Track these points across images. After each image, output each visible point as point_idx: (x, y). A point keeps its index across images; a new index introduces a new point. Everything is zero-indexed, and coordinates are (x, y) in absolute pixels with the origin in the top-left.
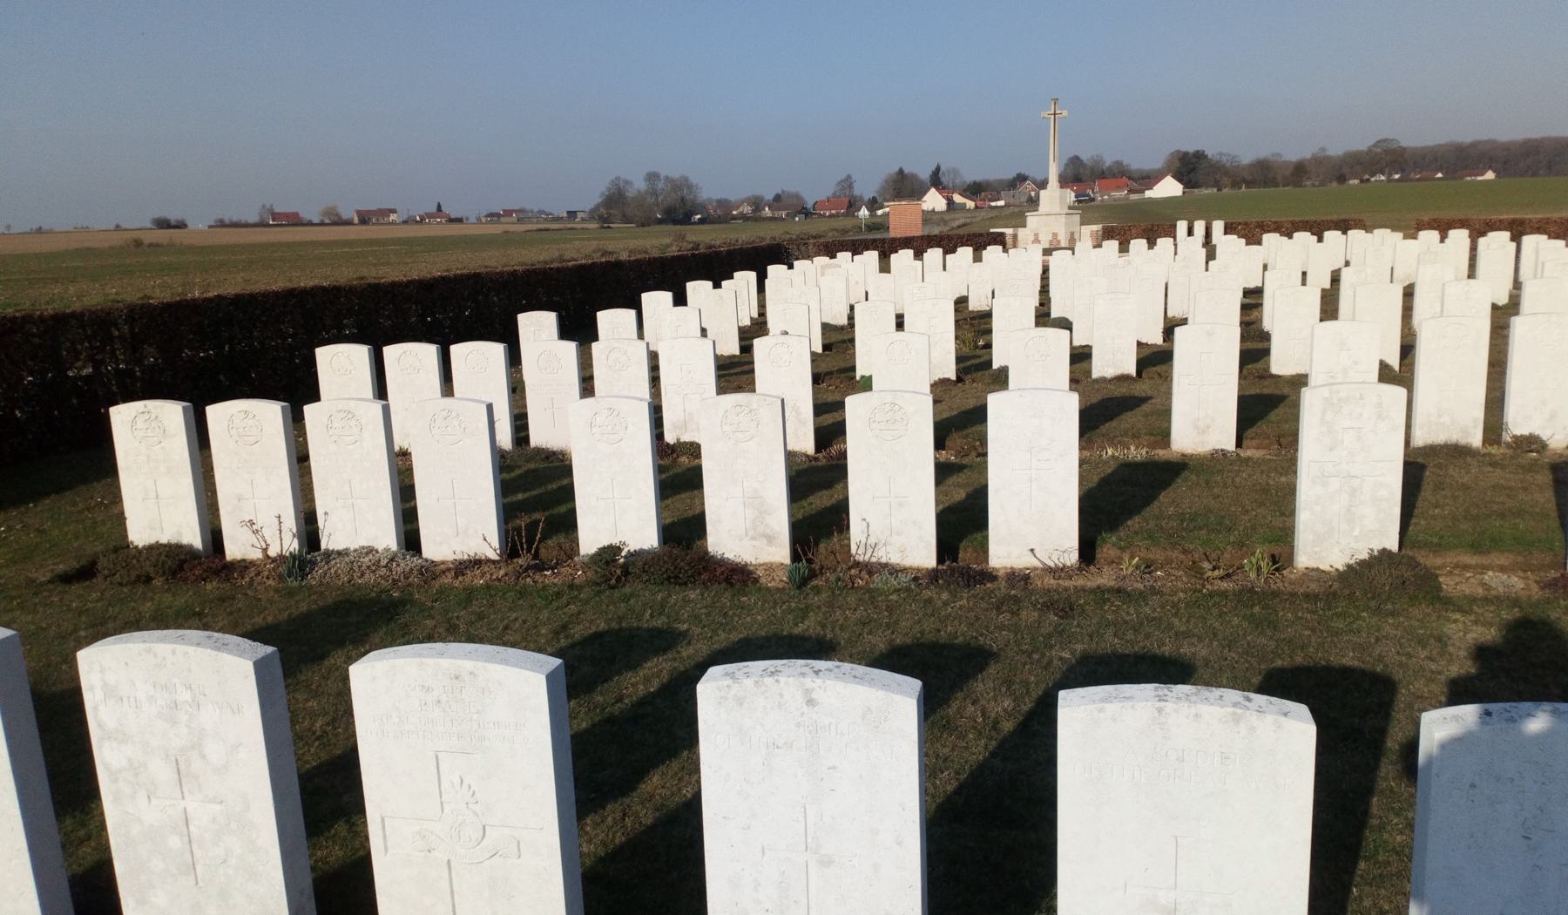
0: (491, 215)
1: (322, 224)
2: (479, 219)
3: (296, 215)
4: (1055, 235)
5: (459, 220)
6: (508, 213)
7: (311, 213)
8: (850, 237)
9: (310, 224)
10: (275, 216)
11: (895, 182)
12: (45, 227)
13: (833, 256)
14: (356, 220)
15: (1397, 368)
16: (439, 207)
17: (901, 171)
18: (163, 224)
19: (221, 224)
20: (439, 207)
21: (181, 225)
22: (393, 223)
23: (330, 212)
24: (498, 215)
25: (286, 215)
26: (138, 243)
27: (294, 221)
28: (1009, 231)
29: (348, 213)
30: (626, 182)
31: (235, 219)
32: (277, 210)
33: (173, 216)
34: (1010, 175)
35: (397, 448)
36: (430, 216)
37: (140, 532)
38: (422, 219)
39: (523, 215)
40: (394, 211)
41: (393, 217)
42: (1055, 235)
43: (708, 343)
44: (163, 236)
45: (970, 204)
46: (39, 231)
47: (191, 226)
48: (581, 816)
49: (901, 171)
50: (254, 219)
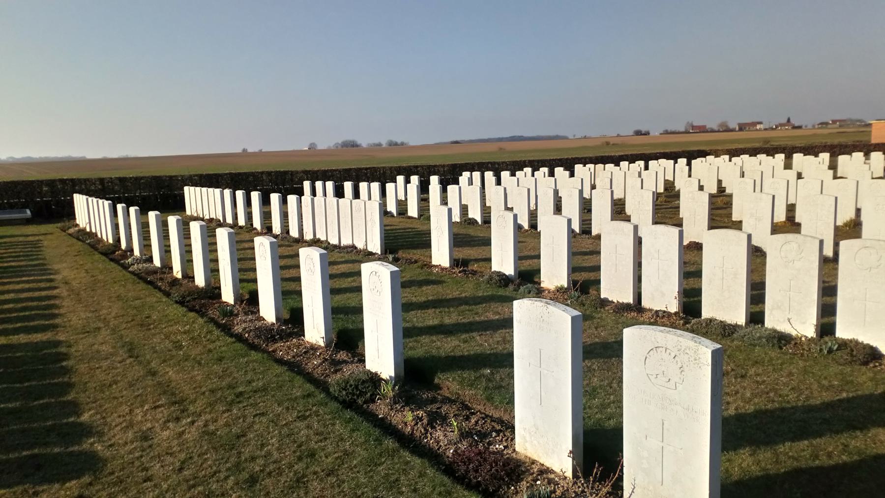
0: (822, 124)
1: (719, 131)
2: (814, 126)
3: (704, 127)
5: (800, 127)
6: (834, 122)
8: (829, 141)
9: (713, 131)
10: (693, 127)
12: (588, 135)
13: (816, 156)
14: (737, 129)
15: (719, 346)
16: (789, 120)
18: (638, 133)
19: (666, 132)
20: (789, 120)
21: (647, 133)
22: (760, 130)
23: (721, 125)
24: (827, 124)
25: (699, 127)
26: (608, 144)
27: (703, 130)
29: (733, 125)
31: (673, 130)
32: (695, 124)
33: (644, 129)
35: (685, 243)
36: (781, 125)
37: (496, 266)
38: (777, 127)
39: (843, 123)
40: (760, 123)
41: (758, 127)
43: (510, 215)
44: (640, 139)
46: (585, 137)
47: (651, 134)
48: (725, 448)
50: (683, 129)
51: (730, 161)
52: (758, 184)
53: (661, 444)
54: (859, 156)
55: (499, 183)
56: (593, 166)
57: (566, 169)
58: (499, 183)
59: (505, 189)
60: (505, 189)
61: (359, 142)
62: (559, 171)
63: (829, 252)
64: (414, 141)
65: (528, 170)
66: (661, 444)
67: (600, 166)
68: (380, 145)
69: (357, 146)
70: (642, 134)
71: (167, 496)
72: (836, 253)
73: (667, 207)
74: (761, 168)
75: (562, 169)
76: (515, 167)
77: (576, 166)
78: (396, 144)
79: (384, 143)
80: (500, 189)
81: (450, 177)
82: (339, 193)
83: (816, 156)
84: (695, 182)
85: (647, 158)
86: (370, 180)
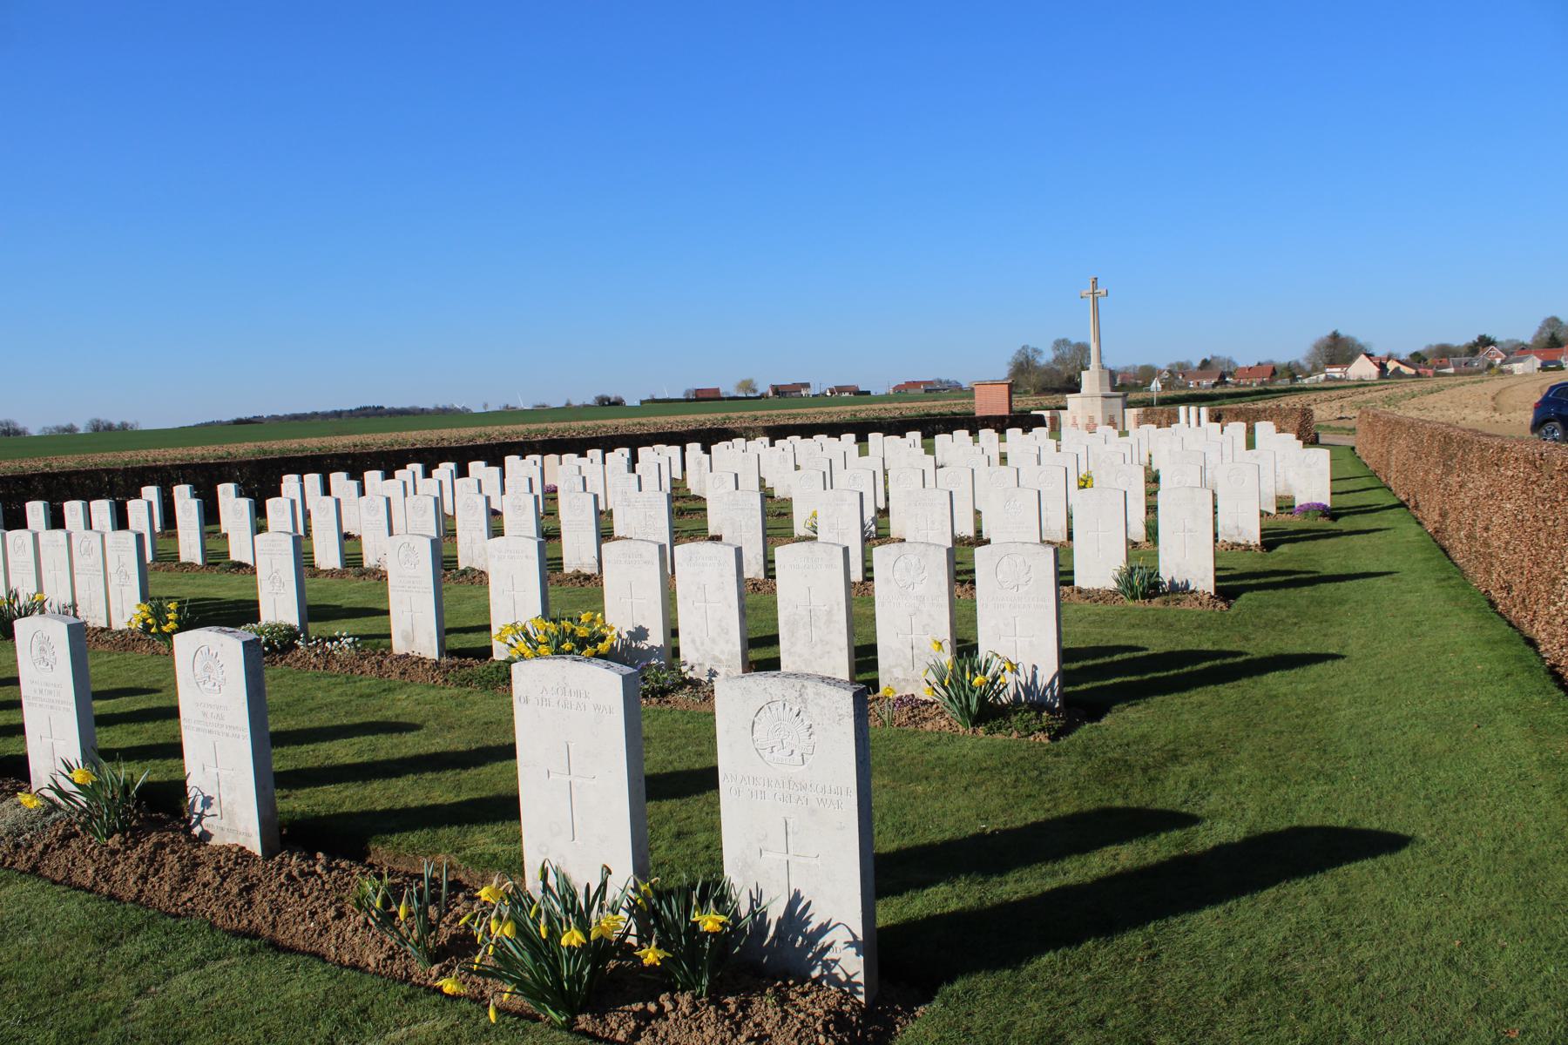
4: (1091, 418)
7: (729, 388)
11: (1329, 347)
13: (903, 436)
17: (1335, 336)
28: (1046, 414)
30: (1035, 350)
33: (613, 396)
34: (1462, 338)
42: (1091, 418)
45: (1413, 372)
49: (1335, 336)
51: (772, 444)
52: (825, 479)
53: (568, 778)
54: (962, 435)
55: (326, 491)
56: (538, 457)
57: (351, 477)
58: (326, 491)
59: (338, 501)
60: (338, 501)
61: (21, 425)
62: (338, 479)
63: (754, 570)
64: (147, 421)
65: (417, 467)
66: (568, 778)
67: (552, 459)
68: (71, 430)
69: (17, 433)
70: (611, 404)
71: (1232, 1025)
72: (770, 572)
73: (687, 515)
74: (827, 454)
75: (343, 475)
76: (390, 462)
77: (285, 478)
78: (109, 428)
79: (82, 427)
80: (330, 501)
81: (260, 482)
82: (56, 520)
83: (903, 436)
84: (728, 477)
85: (634, 442)
86: (88, 496)
